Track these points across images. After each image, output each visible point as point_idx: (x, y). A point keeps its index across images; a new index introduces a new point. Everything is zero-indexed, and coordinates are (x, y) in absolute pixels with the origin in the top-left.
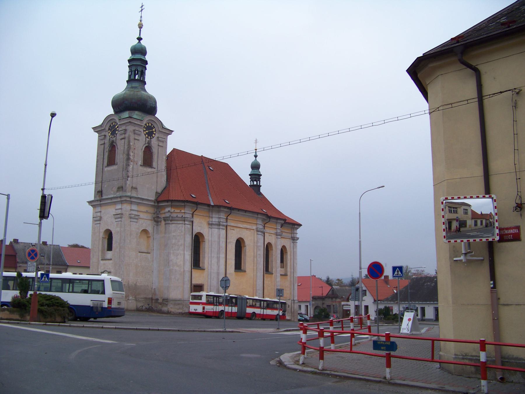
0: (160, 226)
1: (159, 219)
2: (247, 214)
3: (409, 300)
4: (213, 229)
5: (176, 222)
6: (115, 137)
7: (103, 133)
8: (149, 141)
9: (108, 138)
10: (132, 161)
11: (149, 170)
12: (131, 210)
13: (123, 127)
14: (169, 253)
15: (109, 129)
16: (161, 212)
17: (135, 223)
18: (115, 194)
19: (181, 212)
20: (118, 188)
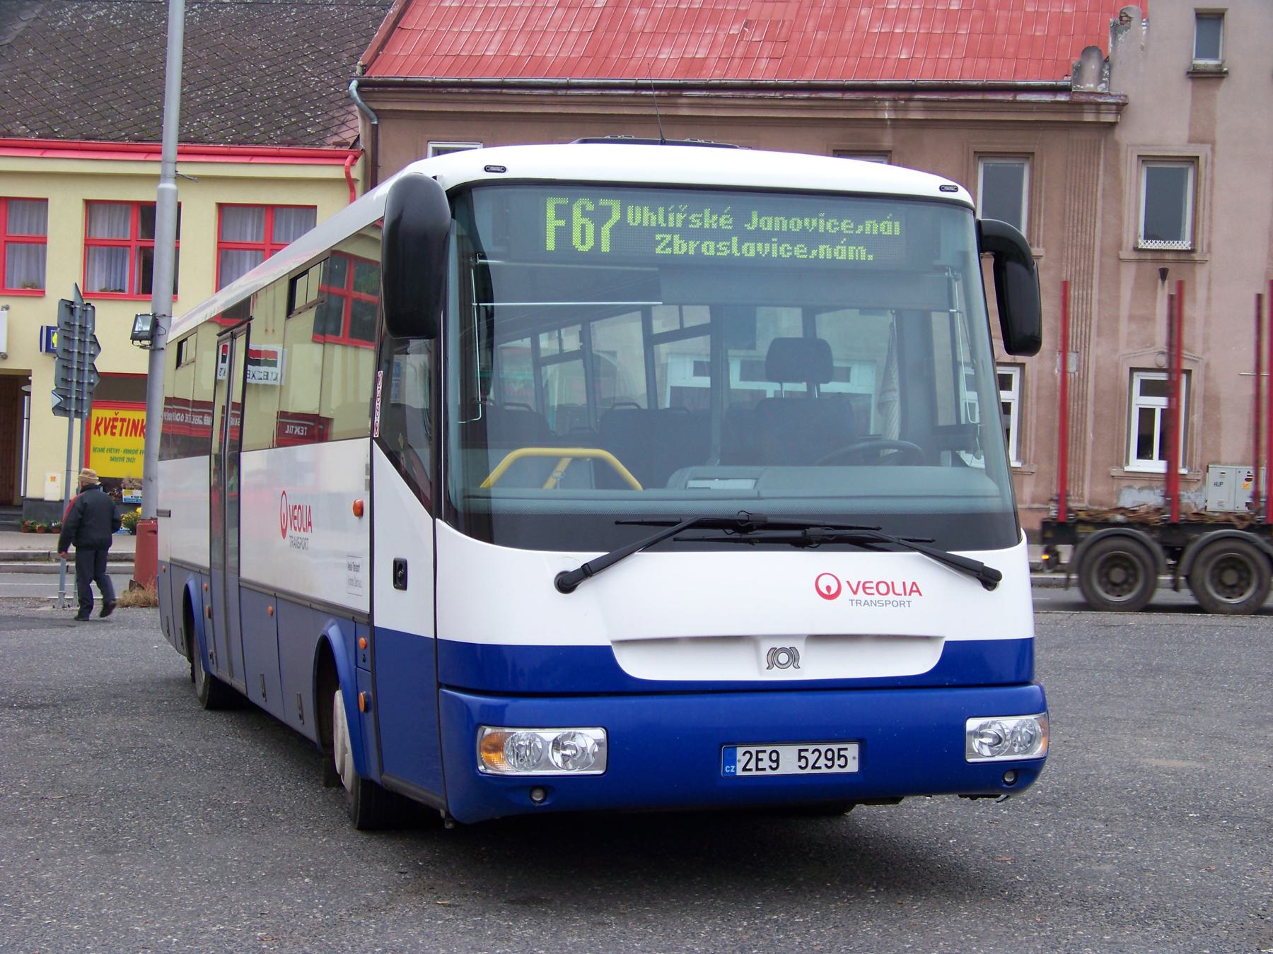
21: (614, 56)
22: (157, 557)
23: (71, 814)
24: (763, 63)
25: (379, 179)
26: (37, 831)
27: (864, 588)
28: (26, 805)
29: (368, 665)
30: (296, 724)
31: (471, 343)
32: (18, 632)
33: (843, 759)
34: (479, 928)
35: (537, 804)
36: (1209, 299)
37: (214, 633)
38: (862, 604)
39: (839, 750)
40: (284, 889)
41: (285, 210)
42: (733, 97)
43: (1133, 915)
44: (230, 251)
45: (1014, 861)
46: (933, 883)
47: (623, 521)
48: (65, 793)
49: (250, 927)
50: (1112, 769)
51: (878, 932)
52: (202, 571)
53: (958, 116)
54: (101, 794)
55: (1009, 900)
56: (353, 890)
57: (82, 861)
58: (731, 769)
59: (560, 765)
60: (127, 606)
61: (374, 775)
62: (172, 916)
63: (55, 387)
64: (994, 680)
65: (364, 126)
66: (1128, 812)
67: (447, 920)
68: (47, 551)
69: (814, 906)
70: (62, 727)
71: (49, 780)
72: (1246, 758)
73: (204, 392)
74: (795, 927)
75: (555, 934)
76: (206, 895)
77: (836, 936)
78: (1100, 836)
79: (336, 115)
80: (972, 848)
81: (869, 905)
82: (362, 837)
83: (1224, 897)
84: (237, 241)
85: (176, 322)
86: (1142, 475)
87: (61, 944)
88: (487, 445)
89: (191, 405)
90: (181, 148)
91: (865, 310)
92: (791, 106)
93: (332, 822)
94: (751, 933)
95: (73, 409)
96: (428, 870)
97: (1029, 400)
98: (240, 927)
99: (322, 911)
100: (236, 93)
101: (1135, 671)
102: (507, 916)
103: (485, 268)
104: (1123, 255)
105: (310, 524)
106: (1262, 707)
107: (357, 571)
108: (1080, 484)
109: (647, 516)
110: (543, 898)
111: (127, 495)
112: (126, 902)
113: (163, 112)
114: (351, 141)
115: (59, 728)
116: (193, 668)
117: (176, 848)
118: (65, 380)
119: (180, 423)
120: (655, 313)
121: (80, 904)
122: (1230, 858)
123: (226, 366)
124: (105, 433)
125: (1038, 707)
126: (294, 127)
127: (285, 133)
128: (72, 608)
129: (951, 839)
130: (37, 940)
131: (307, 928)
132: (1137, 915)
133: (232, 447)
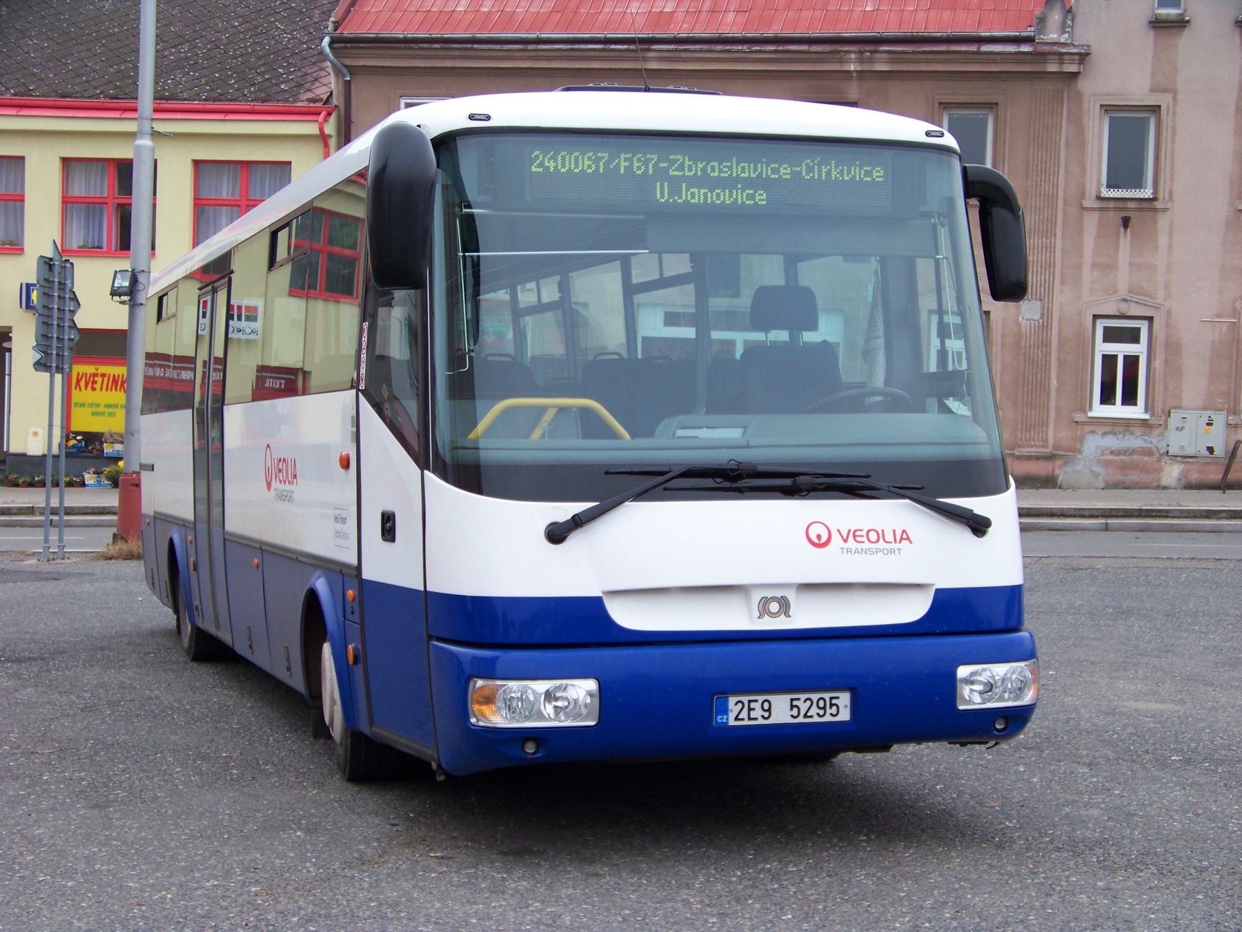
21: (583, 11)
22: (140, 509)
23: (62, 768)
24: (730, 16)
25: (352, 136)
26: (28, 786)
27: (855, 536)
28: (17, 759)
29: (356, 617)
30: (282, 675)
31: (457, 293)
32: (4, 586)
33: (834, 708)
34: (473, 881)
35: (530, 756)
36: (1170, 247)
37: (199, 586)
38: (853, 552)
39: (831, 698)
40: (276, 843)
41: (260, 166)
42: (701, 51)
43: (1124, 860)
44: (206, 208)
45: (1002, 806)
46: (923, 830)
47: (612, 471)
48: (55, 748)
49: (244, 883)
50: (1092, 713)
51: (872, 880)
52: (186, 524)
53: (923, 68)
54: (90, 748)
55: (1000, 846)
56: (344, 843)
57: (74, 816)
58: (723, 719)
59: (552, 716)
60: (111, 559)
61: (364, 727)
62: (165, 871)
63: (35, 344)
64: (984, 627)
65: (337, 82)
66: (1112, 755)
67: (441, 873)
68: (31, 505)
69: (807, 855)
70: (51, 681)
71: (39, 734)
72: (1223, 700)
73: (185, 347)
74: (789, 876)
75: (550, 887)
76: (198, 850)
77: (830, 885)
78: (1086, 780)
79: (309, 71)
80: (960, 794)
81: (861, 853)
82: (352, 789)
83: (1213, 840)
84: (214, 197)
85: (157, 277)
86: (1106, 421)
87: (56, 901)
88: (474, 395)
89: (172, 359)
90: (156, 105)
91: (850, 257)
92: (757, 58)
93: (322, 774)
94: (746, 883)
95: (54, 365)
96: (419, 822)
97: (994, 348)
98: (234, 882)
99: (315, 865)
100: (209, 50)
101: (1106, 614)
102: (501, 868)
103: (471, 217)
104: (1086, 204)
105: (295, 476)
106: (1235, 649)
107: (344, 523)
108: (1045, 429)
109: (636, 465)
110: (536, 849)
111: (108, 449)
112: (120, 858)
113: (138, 69)
114: (325, 97)
115: (47, 682)
116: (178, 620)
117: (167, 802)
118: (45, 337)
119: (160, 378)
120: (634, 260)
121: (73, 860)
122: (1216, 801)
123: (207, 321)
124: (86, 388)
125: (1029, 654)
126: (268, 84)
127: (260, 90)
128: (57, 561)
129: (938, 784)
130: (32, 897)
131: (301, 883)
132: (1128, 860)
133: (214, 401)
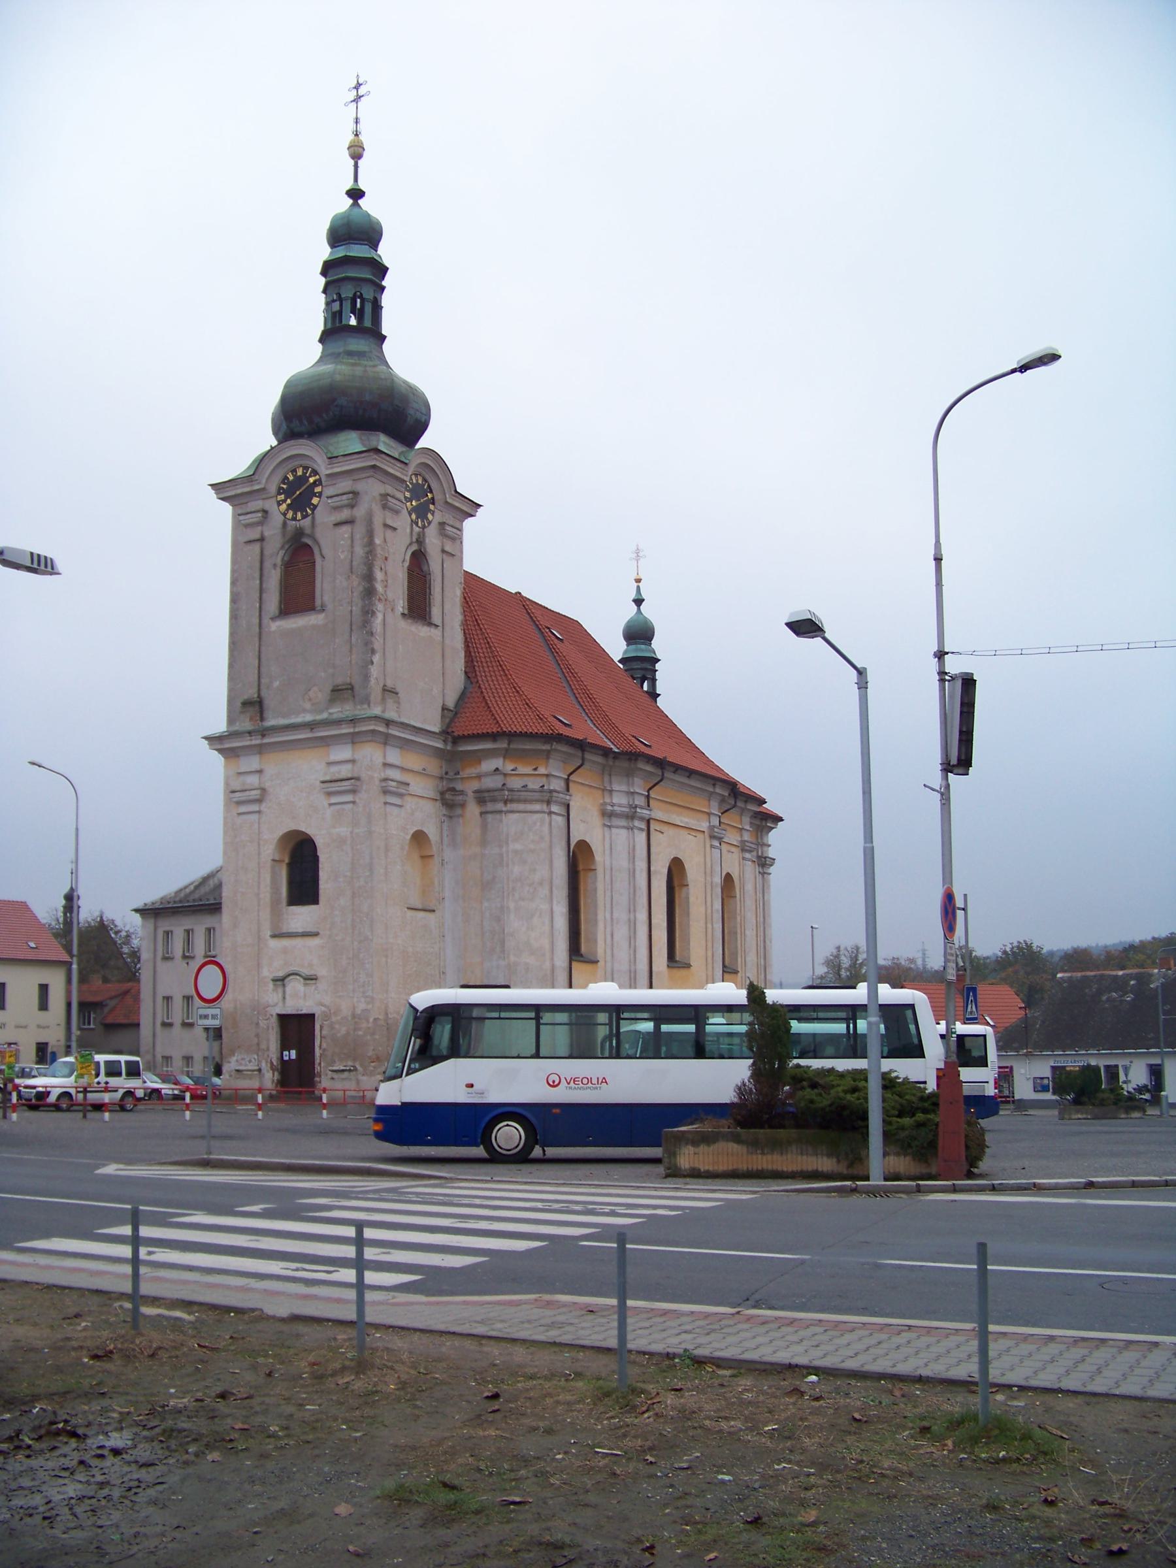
0: (461, 820)
1: (460, 798)
2: (693, 783)
3: (1162, 1045)
4: (614, 830)
5: (521, 807)
6: (309, 518)
7: (257, 504)
8: (419, 534)
9: (277, 519)
10: (380, 600)
11: (423, 631)
12: (385, 765)
13: (345, 485)
14: (502, 907)
15: (280, 488)
16: (464, 774)
17: (396, 810)
18: (321, 712)
19: (536, 773)
20: (333, 691)
27: (574, 1081)
